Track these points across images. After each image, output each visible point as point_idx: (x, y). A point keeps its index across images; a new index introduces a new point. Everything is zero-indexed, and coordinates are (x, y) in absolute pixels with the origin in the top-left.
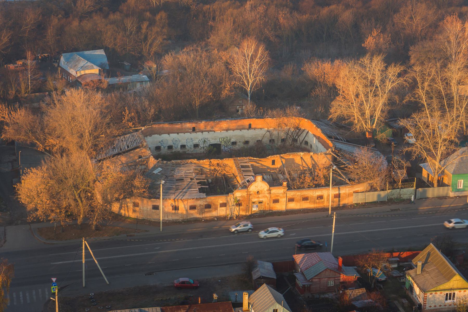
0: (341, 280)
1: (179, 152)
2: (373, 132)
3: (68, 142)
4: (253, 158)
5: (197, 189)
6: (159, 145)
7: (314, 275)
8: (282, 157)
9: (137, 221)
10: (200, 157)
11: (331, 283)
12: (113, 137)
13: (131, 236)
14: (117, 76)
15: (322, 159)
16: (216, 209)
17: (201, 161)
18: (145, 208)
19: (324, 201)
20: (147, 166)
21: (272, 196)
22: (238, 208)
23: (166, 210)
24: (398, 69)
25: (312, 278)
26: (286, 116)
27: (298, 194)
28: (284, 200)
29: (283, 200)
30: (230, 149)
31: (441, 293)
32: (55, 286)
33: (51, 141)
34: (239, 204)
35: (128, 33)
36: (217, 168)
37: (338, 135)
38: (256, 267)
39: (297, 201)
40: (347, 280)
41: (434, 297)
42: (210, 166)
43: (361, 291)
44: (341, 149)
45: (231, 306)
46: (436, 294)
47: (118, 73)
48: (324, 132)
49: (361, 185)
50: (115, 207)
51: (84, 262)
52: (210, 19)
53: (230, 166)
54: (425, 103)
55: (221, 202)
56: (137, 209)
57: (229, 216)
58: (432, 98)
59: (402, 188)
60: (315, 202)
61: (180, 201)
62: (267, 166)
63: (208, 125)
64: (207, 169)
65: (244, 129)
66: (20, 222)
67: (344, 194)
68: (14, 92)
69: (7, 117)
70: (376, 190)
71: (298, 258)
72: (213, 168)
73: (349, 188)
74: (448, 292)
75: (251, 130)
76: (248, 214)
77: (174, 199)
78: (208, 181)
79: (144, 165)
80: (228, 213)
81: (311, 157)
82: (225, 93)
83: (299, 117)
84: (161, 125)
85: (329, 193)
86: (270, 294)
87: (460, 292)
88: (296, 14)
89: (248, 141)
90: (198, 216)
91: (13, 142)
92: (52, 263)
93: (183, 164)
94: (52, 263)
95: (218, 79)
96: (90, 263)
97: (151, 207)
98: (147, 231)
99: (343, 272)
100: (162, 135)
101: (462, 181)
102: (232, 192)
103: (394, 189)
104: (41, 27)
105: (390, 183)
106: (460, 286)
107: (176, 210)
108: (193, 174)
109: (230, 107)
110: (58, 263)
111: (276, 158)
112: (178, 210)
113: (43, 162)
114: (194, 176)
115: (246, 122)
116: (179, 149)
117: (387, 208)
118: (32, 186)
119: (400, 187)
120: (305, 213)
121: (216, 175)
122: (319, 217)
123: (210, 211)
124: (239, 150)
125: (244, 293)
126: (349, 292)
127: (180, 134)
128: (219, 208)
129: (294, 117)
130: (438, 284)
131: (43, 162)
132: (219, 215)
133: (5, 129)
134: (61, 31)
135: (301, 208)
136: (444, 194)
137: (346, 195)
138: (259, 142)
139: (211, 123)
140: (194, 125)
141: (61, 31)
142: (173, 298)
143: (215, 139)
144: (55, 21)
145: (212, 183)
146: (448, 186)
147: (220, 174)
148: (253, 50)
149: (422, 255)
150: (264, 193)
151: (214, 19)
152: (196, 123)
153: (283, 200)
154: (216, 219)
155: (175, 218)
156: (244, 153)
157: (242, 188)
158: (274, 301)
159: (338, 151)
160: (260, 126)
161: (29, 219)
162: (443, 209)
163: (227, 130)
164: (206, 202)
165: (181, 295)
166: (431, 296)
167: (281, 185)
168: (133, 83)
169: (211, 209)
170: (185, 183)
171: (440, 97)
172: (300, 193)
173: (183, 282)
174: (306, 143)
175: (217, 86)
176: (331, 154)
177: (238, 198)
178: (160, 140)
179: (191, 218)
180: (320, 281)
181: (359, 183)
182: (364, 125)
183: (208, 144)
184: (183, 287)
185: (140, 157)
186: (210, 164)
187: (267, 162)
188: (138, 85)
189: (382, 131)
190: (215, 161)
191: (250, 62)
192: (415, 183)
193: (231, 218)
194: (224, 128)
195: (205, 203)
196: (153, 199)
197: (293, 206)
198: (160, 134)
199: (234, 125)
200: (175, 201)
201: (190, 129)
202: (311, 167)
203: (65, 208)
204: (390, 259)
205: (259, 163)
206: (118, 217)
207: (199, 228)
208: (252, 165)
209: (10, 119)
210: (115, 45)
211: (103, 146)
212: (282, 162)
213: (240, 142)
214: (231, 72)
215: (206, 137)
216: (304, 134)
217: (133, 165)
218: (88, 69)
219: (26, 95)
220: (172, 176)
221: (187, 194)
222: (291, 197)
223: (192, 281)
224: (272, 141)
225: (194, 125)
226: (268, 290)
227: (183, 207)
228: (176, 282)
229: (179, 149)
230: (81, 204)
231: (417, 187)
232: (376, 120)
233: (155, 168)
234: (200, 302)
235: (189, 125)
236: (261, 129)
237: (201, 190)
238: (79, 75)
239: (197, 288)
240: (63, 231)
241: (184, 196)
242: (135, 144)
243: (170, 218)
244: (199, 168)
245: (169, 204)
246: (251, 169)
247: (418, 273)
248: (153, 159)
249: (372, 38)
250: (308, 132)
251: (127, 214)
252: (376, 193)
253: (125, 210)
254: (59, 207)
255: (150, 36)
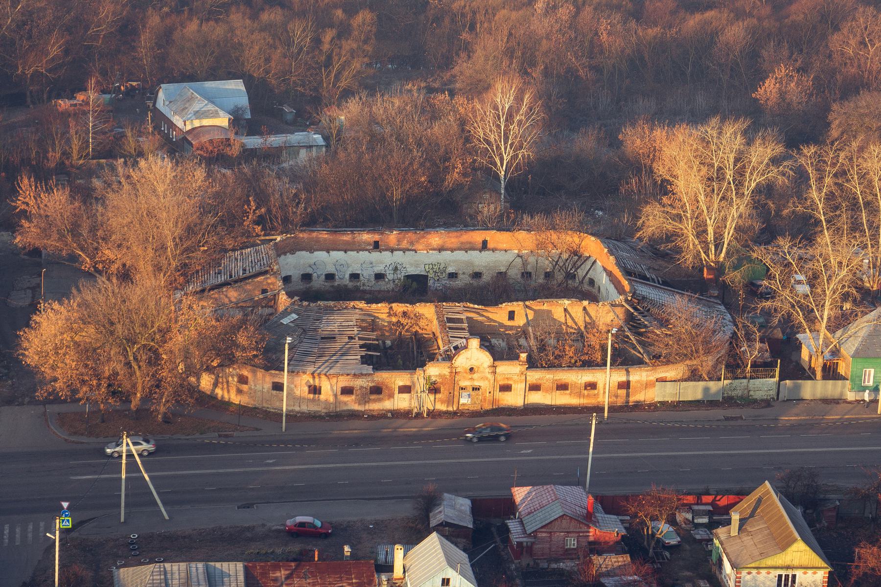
0: (591, 539)
1: (346, 286)
2: (719, 269)
3: (136, 257)
4: (472, 305)
5: (359, 357)
6: (309, 271)
7: (540, 526)
8: (527, 307)
9: (243, 410)
10: (374, 298)
11: (572, 543)
12: (220, 252)
13: (226, 436)
14: (259, 133)
15: (607, 316)
16: (391, 396)
17: (374, 306)
18: (259, 387)
19: (598, 394)
20: (276, 310)
21: (499, 378)
22: (432, 397)
23: (298, 393)
24: (769, 151)
25: (536, 531)
26: (554, 228)
27: (548, 376)
28: (519, 386)
29: (519, 388)
30: (445, 286)
31: (768, 573)
32: (66, 516)
33: (108, 253)
34: (434, 389)
35: (295, 50)
36: (403, 321)
37: (648, 269)
38: (439, 505)
39: (547, 391)
40: (602, 540)
41: (754, 578)
42: (390, 315)
43: (621, 559)
44: (644, 298)
45: (373, 568)
46: (758, 573)
47: (264, 128)
48: (618, 264)
49: (671, 366)
50: (206, 382)
51: (124, 477)
52: (464, 26)
53: (427, 315)
54: (823, 218)
55: (401, 384)
56: (245, 387)
57: (415, 410)
58: (837, 208)
59: (752, 378)
60: (580, 395)
61: (323, 377)
62: (499, 323)
63: (404, 238)
64: (383, 320)
65: (473, 249)
66: (27, 399)
67: (638, 382)
68: (58, 155)
69: (32, 203)
70: (700, 378)
71: (520, 493)
72: (394, 319)
73: (647, 371)
74: (783, 573)
75: (487, 252)
76: (450, 409)
77: (313, 374)
78: (384, 343)
79: (271, 307)
80: (413, 405)
81: (585, 309)
82: (454, 177)
83: (580, 232)
84: (314, 234)
85: (607, 379)
86: (441, 551)
87: (805, 573)
88: (633, 24)
89: (480, 273)
90: (356, 407)
91: (36, 252)
92: (72, 478)
93: (339, 310)
94: (72, 478)
95: (442, 150)
96: (135, 481)
97: (270, 385)
98: (257, 429)
99: (596, 523)
100: (316, 253)
101: (872, 371)
102: (422, 365)
103: (737, 378)
104: (127, 31)
105: (728, 366)
106: (805, 563)
107: (315, 393)
108: (355, 329)
109: (465, 206)
110: (84, 477)
111: (517, 307)
112: (320, 393)
113: (74, 291)
114: (356, 332)
115: (478, 237)
116: (346, 280)
117: (718, 413)
118: (50, 336)
119: (748, 375)
120: (561, 413)
121: (400, 333)
122: (566, 423)
123: (380, 400)
124: (460, 289)
125: (397, 546)
126: (597, 560)
127: (349, 253)
128: (396, 395)
129: (570, 232)
130: (763, 555)
131: (74, 291)
132: (396, 408)
133: (22, 226)
134: (166, 37)
135: (553, 403)
136: (836, 395)
137: (642, 385)
138: (502, 275)
139: (411, 235)
140: (377, 237)
141: (166, 37)
142: (279, 551)
143: (417, 266)
144: (154, 20)
145: (391, 348)
146: (845, 379)
147: (407, 331)
148: (512, 98)
149: (747, 503)
150: (483, 372)
151: (472, 28)
152: (382, 234)
153: (519, 388)
154: (389, 415)
155: (313, 408)
156: (468, 296)
157: (444, 360)
158: (445, 563)
159: (637, 301)
160: (504, 246)
161: (40, 394)
162: (823, 420)
163: (440, 249)
164: (373, 381)
165: (296, 547)
166: (748, 577)
167: (517, 358)
168: (293, 150)
169: (381, 396)
170: (338, 345)
171: (854, 206)
172: (551, 376)
173: (302, 524)
174: (592, 282)
175: (438, 162)
176: (623, 306)
177: (433, 379)
178: (312, 262)
179: (344, 411)
180: (550, 537)
181: (668, 362)
182: (703, 255)
183: (403, 274)
184: (302, 532)
185: (264, 291)
186: (389, 313)
187: (498, 314)
188: (303, 153)
189: (736, 267)
190: (399, 308)
191: (507, 120)
192: (778, 370)
193: (419, 415)
194: (435, 246)
195: (371, 385)
196: (273, 372)
197: (536, 398)
198: (311, 250)
199: (453, 240)
200: (314, 377)
201: (369, 244)
202: (582, 328)
203: (109, 378)
204: (696, 507)
205: (483, 316)
206: (209, 401)
207: (354, 429)
208: (467, 318)
209: (39, 207)
210: (268, 73)
211: (200, 268)
212: (526, 315)
213: (464, 273)
214: (468, 140)
215: (400, 261)
216: (588, 264)
217: (247, 307)
218: (207, 117)
219: (81, 162)
220: (315, 330)
221: (338, 365)
222: (535, 382)
223: (318, 523)
224: (526, 275)
225: (377, 237)
226: (438, 543)
227: (329, 388)
228: (289, 522)
229: (346, 280)
230: (138, 373)
231: (782, 378)
232: (725, 246)
233: (286, 313)
234: (316, 559)
235: (366, 237)
236: (506, 251)
237: (365, 360)
238: (189, 127)
239: (327, 535)
240: (103, 421)
241: (331, 368)
242: (257, 268)
243: (304, 408)
244: (369, 319)
245: (304, 382)
246: (465, 325)
247: (732, 534)
248: (285, 297)
249: (773, 81)
250: (595, 262)
251: (226, 396)
252: (702, 384)
253: (222, 389)
254: (98, 377)
255: (336, 58)
